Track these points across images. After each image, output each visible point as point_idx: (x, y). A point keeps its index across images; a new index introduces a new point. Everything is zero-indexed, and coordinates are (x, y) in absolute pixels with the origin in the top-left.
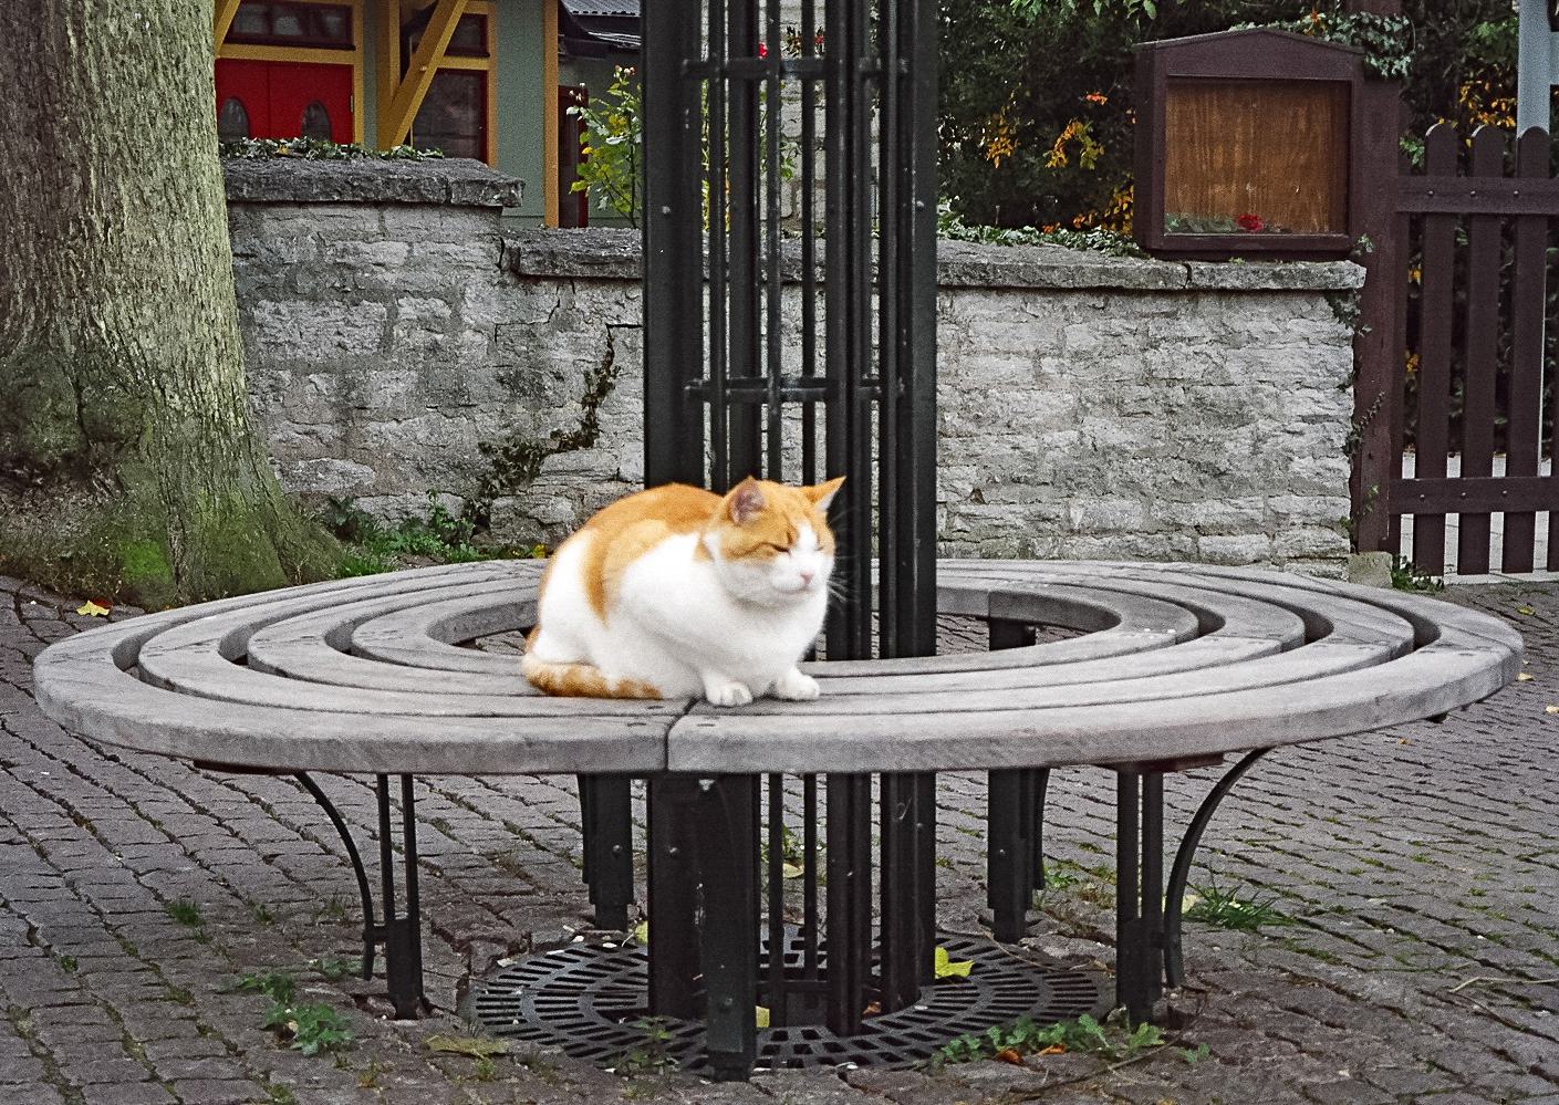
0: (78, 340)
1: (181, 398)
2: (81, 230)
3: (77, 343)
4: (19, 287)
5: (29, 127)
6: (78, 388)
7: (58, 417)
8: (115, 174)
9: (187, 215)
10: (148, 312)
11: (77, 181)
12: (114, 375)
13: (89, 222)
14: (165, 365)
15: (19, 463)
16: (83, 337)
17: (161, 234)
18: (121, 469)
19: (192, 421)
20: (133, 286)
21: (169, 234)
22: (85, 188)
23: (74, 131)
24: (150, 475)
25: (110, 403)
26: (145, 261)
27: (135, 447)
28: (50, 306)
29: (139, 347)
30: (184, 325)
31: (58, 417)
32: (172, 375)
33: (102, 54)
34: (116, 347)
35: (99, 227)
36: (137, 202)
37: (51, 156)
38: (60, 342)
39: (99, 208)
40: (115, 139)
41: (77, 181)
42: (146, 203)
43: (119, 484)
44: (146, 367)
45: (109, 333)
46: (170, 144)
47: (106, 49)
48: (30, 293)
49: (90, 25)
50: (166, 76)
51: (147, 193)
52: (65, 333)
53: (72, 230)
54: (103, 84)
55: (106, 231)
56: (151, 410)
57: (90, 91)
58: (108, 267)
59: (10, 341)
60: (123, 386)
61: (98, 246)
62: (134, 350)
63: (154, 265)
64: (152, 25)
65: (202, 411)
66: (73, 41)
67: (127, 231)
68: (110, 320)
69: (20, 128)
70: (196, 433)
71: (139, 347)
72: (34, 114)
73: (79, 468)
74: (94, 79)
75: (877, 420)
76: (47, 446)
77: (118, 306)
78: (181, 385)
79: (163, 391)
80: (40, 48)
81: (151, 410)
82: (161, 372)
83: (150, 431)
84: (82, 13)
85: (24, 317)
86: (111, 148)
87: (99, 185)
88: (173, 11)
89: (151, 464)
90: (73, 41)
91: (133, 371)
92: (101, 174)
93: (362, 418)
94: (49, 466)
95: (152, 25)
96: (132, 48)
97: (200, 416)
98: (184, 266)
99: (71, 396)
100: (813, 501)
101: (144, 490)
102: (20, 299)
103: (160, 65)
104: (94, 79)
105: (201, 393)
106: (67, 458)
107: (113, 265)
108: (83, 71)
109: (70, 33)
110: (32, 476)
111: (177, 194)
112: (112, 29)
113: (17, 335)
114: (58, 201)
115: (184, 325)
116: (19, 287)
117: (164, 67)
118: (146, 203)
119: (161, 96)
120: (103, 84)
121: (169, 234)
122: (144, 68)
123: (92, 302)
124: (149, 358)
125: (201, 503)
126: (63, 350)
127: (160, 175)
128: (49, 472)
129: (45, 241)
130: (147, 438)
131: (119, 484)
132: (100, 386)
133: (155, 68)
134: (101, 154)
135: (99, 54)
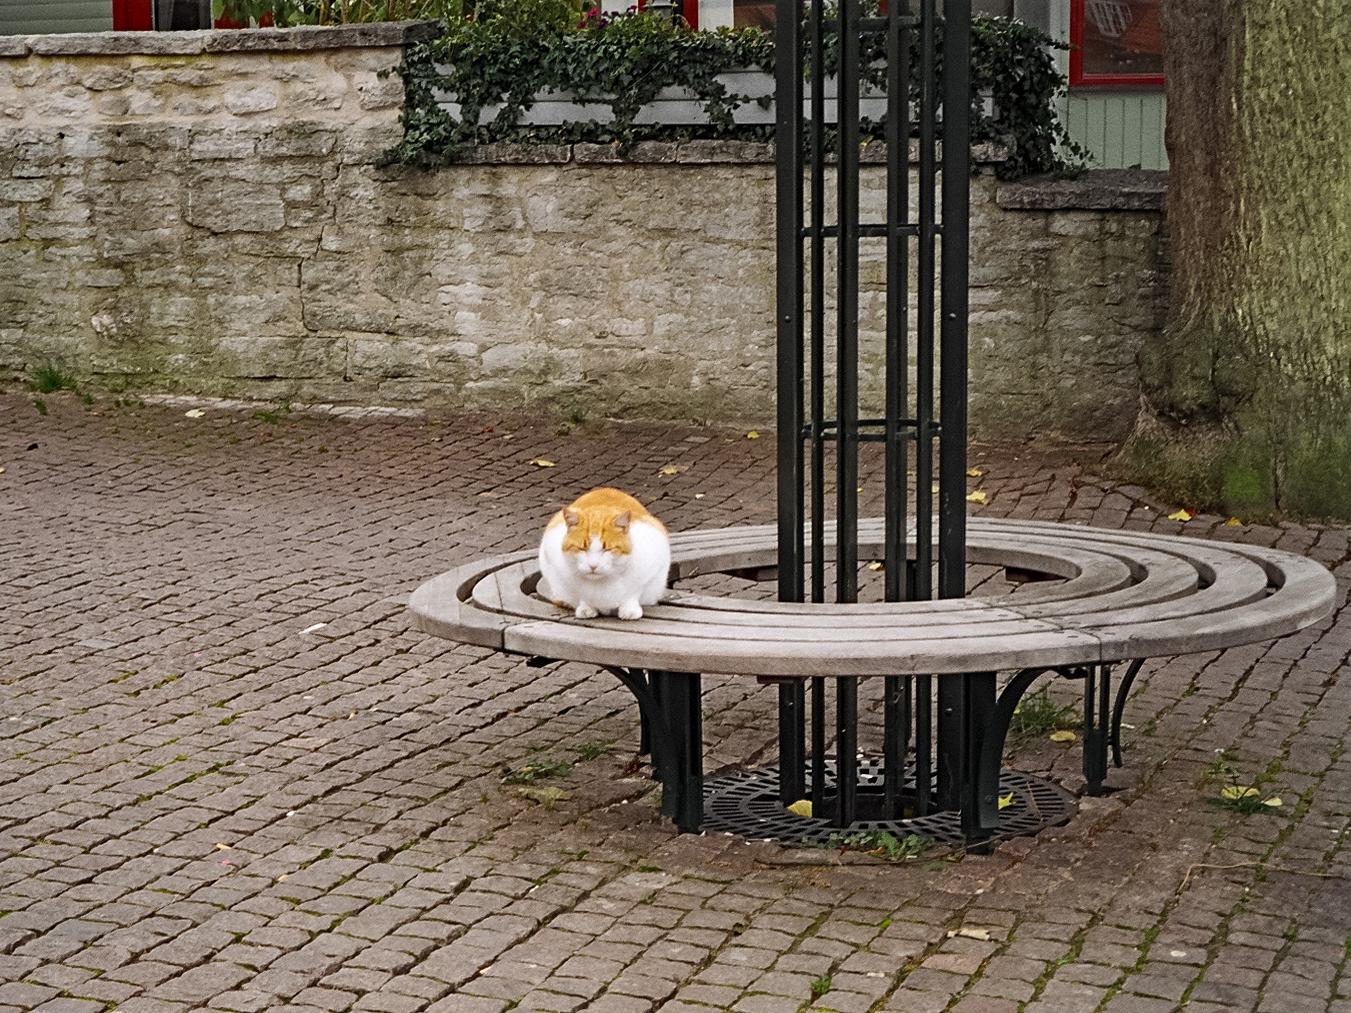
0: (1223, 322)
1: (1293, 367)
2: (1231, 243)
3: (1221, 324)
4: (1193, 282)
5: (1206, 169)
6: (1216, 356)
7: (1194, 378)
8: (1258, 202)
9: (1314, 231)
10: (1274, 303)
11: (1232, 207)
12: (1241, 348)
13: (1237, 237)
14: (1284, 342)
15: (1172, 408)
16: (1226, 320)
17: (1290, 246)
18: (1238, 416)
19: (1302, 383)
20: (1265, 284)
21: (1297, 246)
22: (1237, 212)
23: (1232, 173)
24: (1261, 421)
25: (1234, 369)
26: (1276, 266)
27: (1250, 400)
28: (1209, 297)
29: (1265, 328)
30: (1302, 312)
31: (1194, 378)
32: (1287, 347)
33: (1254, 115)
34: (1247, 328)
35: (1244, 240)
36: (1273, 223)
37: (1217, 191)
38: (1211, 323)
39: (1245, 228)
40: (1259, 177)
41: (1232, 207)
42: (1280, 223)
43: (1237, 428)
44: (1268, 342)
45: (1244, 318)
46: (1304, 179)
47: (1257, 111)
48: (1198, 287)
49: (1246, 94)
50: (1304, 129)
51: (1281, 216)
52: (1216, 319)
53: (1227, 243)
54: (1254, 137)
55: (1248, 243)
56: (1266, 374)
57: (1243, 142)
58: (1248, 270)
59: (1183, 321)
60: (1246, 357)
61: (1243, 255)
62: (1260, 331)
63: (1282, 269)
64: (1295, 91)
65: (1313, 376)
66: (1235, 106)
67: (1263, 244)
68: (1246, 309)
69: (1200, 169)
70: (1304, 392)
71: (1265, 328)
72: (1209, 160)
73: (1212, 414)
74: (1248, 133)
75: (806, 467)
76: (1186, 398)
77: (1253, 298)
78: (1295, 357)
79: (1279, 361)
80: (1215, 112)
81: (1266, 374)
82: (1279, 347)
83: (1263, 390)
84: (1241, 86)
85: (1192, 305)
86: (1257, 183)
87: (1247, 210)
88: (1316, 79)
89: (1262, 413)
90: (1235, 106)
91: (1257, 346)
92: (1248, 202)
93: (1267, 335)
94: (1188, 412)
95: (1295, 91)
96: (1278, 110)
97: (1309, 379)
98: (1307, 269)
99: (1205, 363)
100: (389, 219)
101: (1254, 431)
102: (1192, 291)
103: (1298, 121)
104: (1248, 133)
105: (1313, 363)
106: (1203, 406)
107: (1252, 268)
108: (1240, 128)
109: (1233, 100)
110: (1180, 419)
111: (1306, 216)
112: (1263, 96)
113: (1187, 317)
114: (1220, 221)
115: (1302, 312)
116: (1193, 282)
117: (1303, 123)
118: (1280, 223)
119: (1298, 144)
120: (1254, 137)
121: (1297, 246)
122: (1286, 125)
123: (1235, 295)
124: (1271, 336)
125: (1303, 444)
126: (1212, 329)
127: (1292, 202)
128: (1190, 416)
129: (1209, 250)
130: (1260, 395)
131: (1237, 428)
132: (1230, 356)
133: (1294, 123)
134: (1249, 188)
135: (1252, 114)
